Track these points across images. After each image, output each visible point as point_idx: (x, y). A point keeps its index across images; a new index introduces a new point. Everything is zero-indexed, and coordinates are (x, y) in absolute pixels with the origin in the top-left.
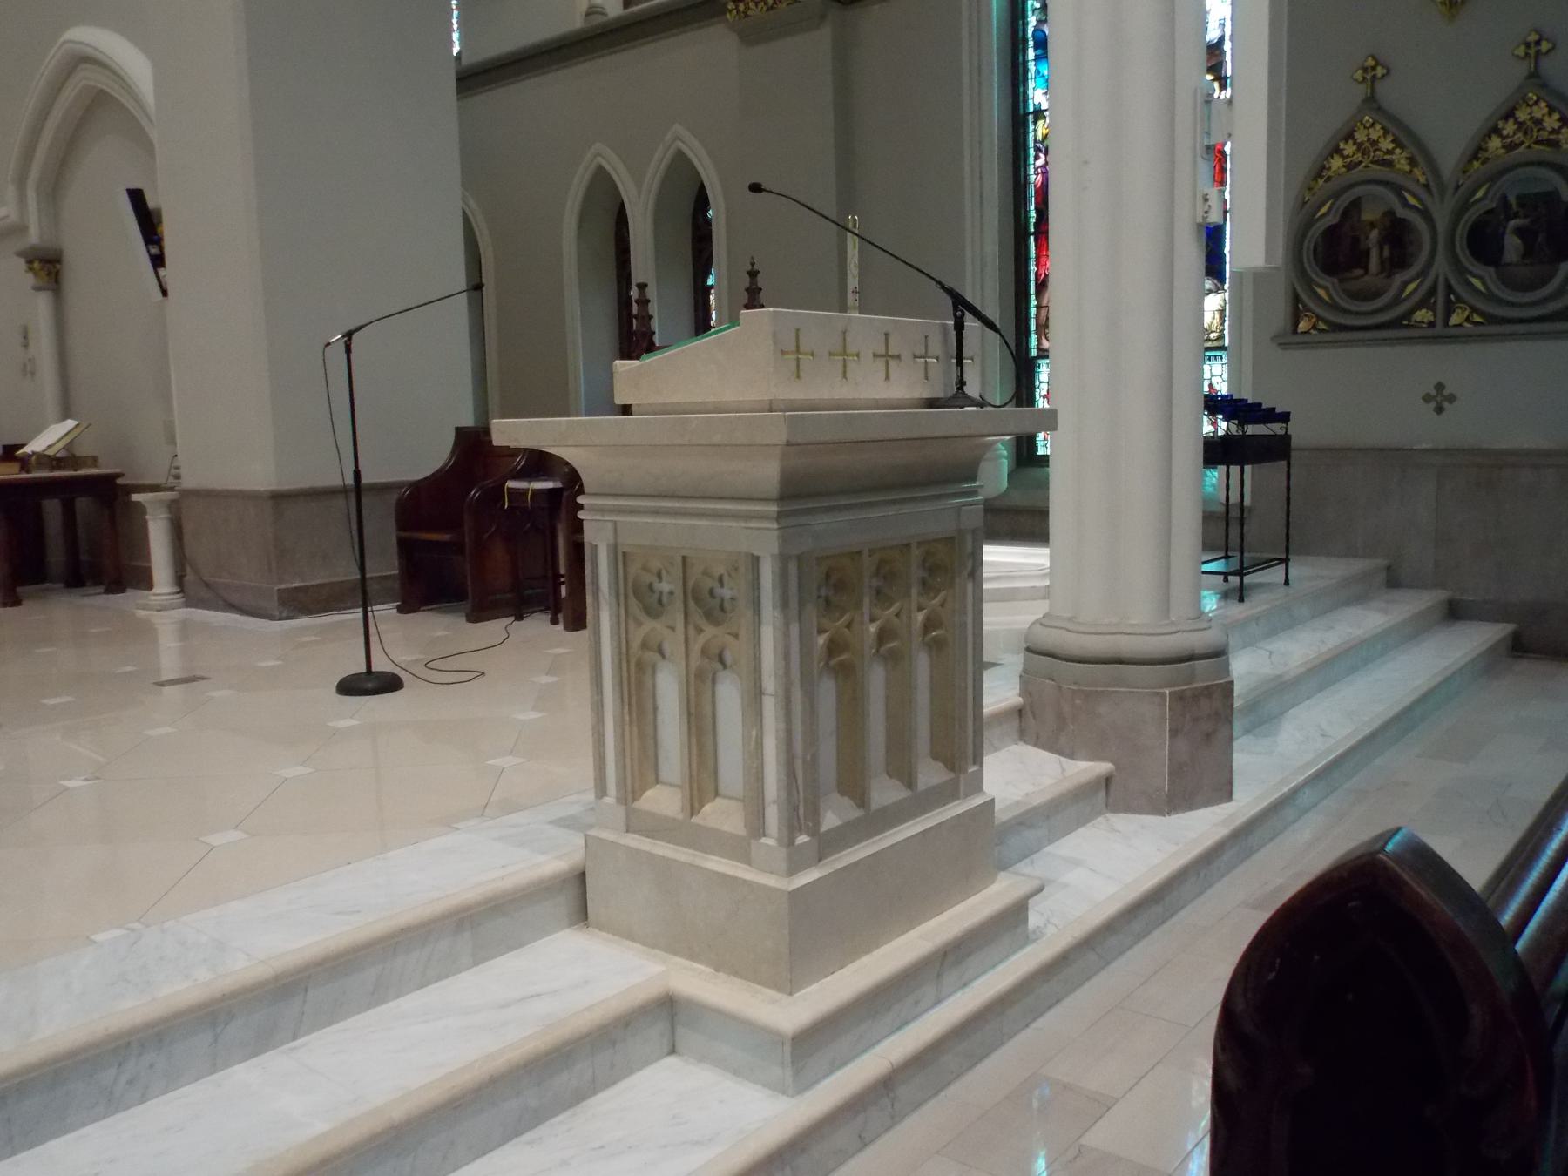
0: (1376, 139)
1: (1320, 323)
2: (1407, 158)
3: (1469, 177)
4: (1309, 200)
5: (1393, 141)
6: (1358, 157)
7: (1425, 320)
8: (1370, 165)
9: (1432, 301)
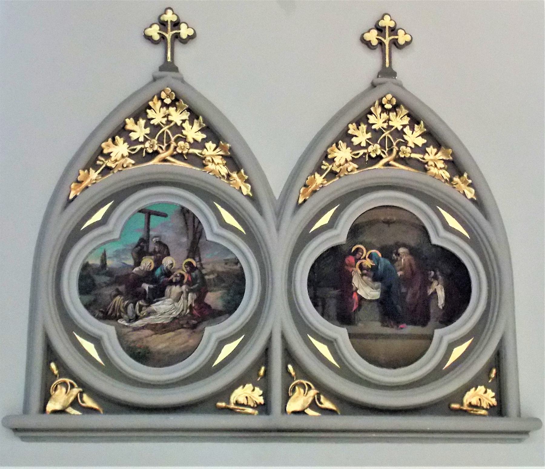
0: (400, 128)
1: (85, 397)
2: (445, 161)
3: (314, 192)
4: (76, 197)
5: (202, 130)
6: (375, 149)
7: (484, 405)
8: (392, 163)
9: (262, 372)
